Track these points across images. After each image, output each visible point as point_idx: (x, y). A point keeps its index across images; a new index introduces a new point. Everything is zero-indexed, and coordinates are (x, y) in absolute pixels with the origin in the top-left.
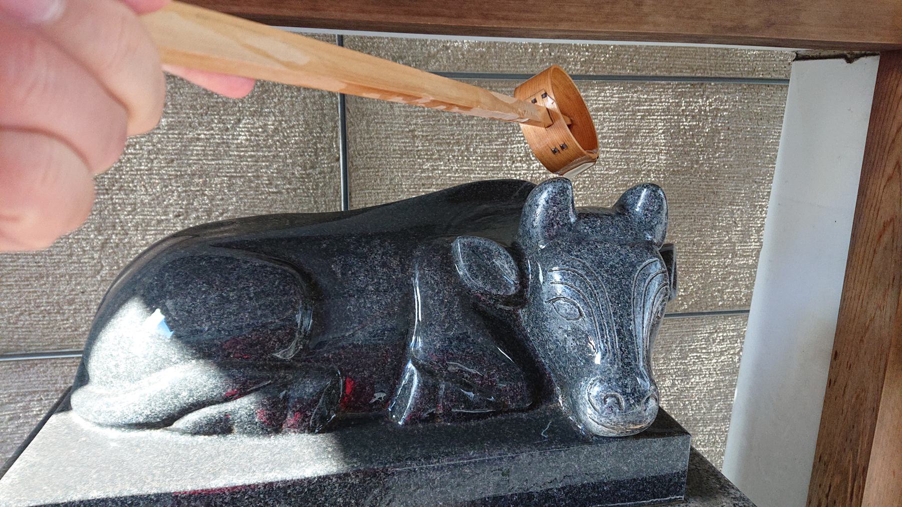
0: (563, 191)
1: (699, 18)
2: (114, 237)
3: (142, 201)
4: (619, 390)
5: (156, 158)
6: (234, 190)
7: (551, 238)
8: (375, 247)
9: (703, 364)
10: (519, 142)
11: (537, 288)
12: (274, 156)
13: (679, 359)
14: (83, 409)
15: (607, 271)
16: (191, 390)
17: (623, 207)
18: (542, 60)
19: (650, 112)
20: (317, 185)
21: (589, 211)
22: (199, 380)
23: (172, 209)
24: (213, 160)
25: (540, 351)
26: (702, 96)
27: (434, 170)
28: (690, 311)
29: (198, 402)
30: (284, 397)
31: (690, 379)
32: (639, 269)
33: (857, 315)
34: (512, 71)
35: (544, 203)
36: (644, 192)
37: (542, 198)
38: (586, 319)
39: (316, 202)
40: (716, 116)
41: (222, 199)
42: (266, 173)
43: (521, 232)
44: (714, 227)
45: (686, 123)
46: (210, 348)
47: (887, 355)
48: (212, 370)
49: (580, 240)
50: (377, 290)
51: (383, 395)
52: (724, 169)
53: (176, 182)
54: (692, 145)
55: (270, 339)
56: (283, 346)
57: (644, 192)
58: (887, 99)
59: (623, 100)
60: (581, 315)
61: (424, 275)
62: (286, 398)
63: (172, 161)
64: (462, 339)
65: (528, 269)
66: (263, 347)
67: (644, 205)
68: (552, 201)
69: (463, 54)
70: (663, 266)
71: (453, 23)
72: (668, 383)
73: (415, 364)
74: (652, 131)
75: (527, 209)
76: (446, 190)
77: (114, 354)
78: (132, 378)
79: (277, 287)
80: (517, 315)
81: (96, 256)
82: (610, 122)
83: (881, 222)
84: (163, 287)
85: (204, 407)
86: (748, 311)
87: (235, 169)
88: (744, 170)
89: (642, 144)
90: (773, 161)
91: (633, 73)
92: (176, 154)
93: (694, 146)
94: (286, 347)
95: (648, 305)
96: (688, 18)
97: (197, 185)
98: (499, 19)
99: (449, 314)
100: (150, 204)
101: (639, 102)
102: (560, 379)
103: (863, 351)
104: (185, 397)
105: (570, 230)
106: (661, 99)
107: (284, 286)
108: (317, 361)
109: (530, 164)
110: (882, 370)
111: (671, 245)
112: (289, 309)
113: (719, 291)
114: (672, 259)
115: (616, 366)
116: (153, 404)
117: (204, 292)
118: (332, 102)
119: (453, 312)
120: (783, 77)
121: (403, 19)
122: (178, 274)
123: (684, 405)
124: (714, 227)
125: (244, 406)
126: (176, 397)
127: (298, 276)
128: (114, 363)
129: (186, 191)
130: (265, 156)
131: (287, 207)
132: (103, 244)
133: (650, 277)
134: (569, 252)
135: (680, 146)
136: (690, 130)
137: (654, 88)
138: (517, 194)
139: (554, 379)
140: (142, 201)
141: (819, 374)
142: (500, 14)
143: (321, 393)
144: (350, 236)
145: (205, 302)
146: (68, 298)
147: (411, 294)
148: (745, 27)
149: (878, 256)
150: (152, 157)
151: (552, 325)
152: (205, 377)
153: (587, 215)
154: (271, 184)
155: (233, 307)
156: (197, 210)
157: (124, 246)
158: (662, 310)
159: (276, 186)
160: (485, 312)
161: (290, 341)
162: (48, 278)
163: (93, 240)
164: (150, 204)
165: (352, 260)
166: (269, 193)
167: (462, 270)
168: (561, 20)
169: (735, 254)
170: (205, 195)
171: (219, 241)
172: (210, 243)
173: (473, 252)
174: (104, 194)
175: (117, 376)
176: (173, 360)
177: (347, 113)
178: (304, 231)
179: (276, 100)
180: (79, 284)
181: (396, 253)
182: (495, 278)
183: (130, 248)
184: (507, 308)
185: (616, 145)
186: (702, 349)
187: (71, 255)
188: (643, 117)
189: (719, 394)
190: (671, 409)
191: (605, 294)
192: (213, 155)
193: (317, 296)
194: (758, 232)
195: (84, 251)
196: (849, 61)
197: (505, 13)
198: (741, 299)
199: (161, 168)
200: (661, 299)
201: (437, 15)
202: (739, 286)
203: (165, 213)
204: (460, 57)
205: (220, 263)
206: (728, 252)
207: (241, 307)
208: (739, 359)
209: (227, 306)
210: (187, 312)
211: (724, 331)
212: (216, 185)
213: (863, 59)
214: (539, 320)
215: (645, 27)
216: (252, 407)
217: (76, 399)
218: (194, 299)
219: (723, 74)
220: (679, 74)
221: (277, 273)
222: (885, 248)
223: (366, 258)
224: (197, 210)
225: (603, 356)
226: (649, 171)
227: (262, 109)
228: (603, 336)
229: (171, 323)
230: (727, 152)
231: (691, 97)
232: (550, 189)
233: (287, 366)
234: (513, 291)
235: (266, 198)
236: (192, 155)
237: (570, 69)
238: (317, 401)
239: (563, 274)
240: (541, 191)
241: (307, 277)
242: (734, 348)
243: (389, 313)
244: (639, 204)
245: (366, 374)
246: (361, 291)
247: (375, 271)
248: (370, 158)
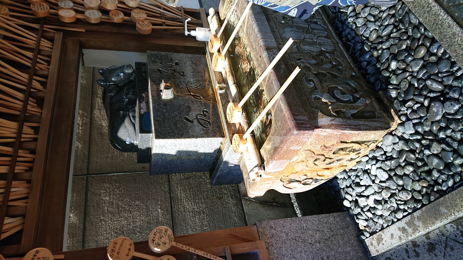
59: (98, 109)
101: (99, 105)
104: (130, 123)
125: (131, 114)
166: (124, 191)
199: (116, 218)
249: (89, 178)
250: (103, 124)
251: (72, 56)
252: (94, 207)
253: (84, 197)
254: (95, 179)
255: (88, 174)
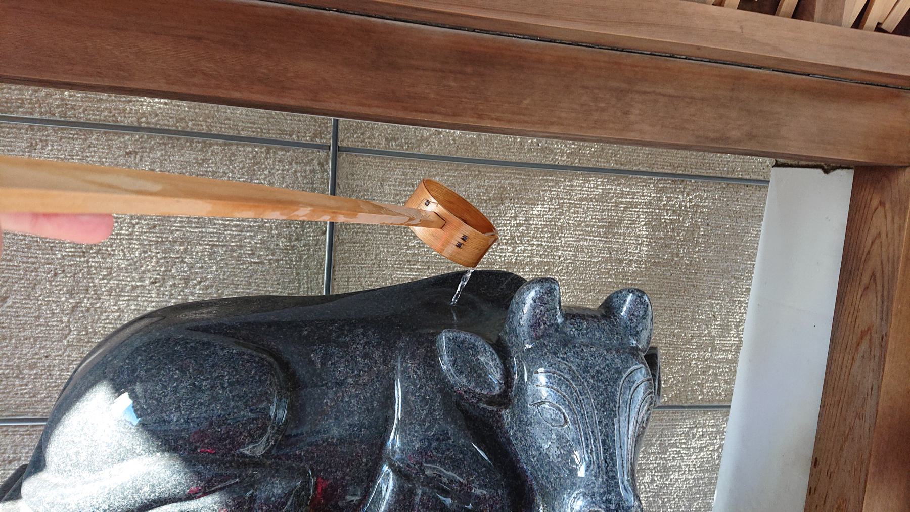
0: (550, 291)
1: (683, 129)
2: (86, 301)
3: (119, 265)
4: (602, 506)
5: (137, 224)
6: (215, 259)
7: (538, 338)
8: (358, 336)
9: (682, 460)
10: (505, 225)
11: (521, 390)
12: (259, 227)
13: (658, 453)
14: (34, 500)
15: (593, 377)
16: (153, 486)
17: (609, 309)
18: (530, 150)
19: (632, 205)
20: (301, 258)
21: (575, 311)
22: (162, 475)
23: (149, 275)
24: (196, 227)
25: (522, 456)
26: (682, 192)
27: (420, 247)
28: (670, 404)
29: (159, 499)
30: (249, 498)
31: (669, 475)
32: (625, 375)
33: (837, 422)
34: (501, 158)
35: (532, 302)
36: (630, 297)
37: (530, 296)
38: (571, 427)
39: (298, 274)
40: (696, 211)
41: (202, 268)
42: (250, 243)
43: (507, 328)
44: (694, 320)
45: (667, 217)
46: (176, 441)
47: (868, 466)
48: (177, 465)
49: (567, 342)
50: (356, 383)
51: (356, 499)
52: (705, 265)
53: (156, 248)
54: (673, 238)
55: (241, 433)
56: (254, 441)
57: (630, 297)
58: (862, 212)
59: (606, 192)
60: (566, 422)
61: (407, 368)
62: (252, 499)
63: (155, 227)
64: (442, 437)
65: (513, 368)
66: (232, 443)
67: (630, 310)
68: (539, 300)
69: (454, 140)
70: (648, 374)
71: (449, 121)
72: (647, 479)
73: (391, 466)
74: (634, 222)
75: (515, 306)
76: (433, 278)
77: (76, 440)
78: (93, 469)
79: (253, 377)
80: (501, 416)
81: (65, 319)
82: (593, 211)
83: (858, 331)
84: (134, 371)
85: (165, 504)
86: (729, 407)
87: (219, 237)
88: (724, 265)
89: (624, 234)
90: (752, 257)
91: (618, 167)
92: (159, 220)
93: (675, 239)
94: (256, 442)
95: (633, 414)
96: (673, 128)
97: (178, 252)
98: (492, 119)
99: (431, 412)
100: (126, 269)
101: (623, 194)
102: (542, 487)
103: (843, 460)
105: (556, 330)
106: (644, 192)
107: (260, 376)
108: (288, 458)
109: (514, 248)
110: (863, 480)
111: (655, 348)
112: (262, 402)
113: (698, 384)
114: (656, 364)
115: (600, 479)
116: (112, 498)
117: (176, 380)
118: (322, 178)
119: (434, 410)
120: (761, 178)
121: (401, 115)
122: (151, 358)
123: (663, 502)
124: (694, 320)
126: (137, 491)
127: (275, 365)
128: (75, 450)
129: (165, 258)
130: (250, 227)
131: (268, 278)
132: (73, 307)
133: (635, 385)
134: (555, 354)
135: (661, 238)
136: (671, 223)
137: (637, 183)
138: (504, 286)
139: (535, 487)
140: (119, 265)
141: (800, 481)
142: (493, 115)
143: (290, 494)
144: (333, 322)
145: (176, 391)
146: (29, 362)
147: (391, 388)
148: (728, 138)
149: (858, 363)
150: (134, 222)
151: (537, 430)
152: (169, 472)
153: (574, 316)
154: (253, 254)
155: (205, 397)
156: (174, 278)
157: (95, 310)
158: (647, 419)
159: (259, 257)
160: (466, 411)
161: (261, 436)
162: (11, 340)
163: (63, 303)
164: (126, 269)
165: (333, 349)
167: (445, 365)
168: (552, 124)
169: (714, 348)
170: (185, 262)
171: (195, 324)
172: (188, 325)
173: (458, 347)
174: (80, 257)
175: (77, 465)
176: (137, 451)
177: (337, 188)
178: (287, 315)
179: (266, 172)
180: (43, 348)
181: (379, 344)
182: (479, 376)
183: (101, 313)
184: (490, 408)
185: (599, 233)
186: (681, 444)
187: (38, 317)
188: (625, 209)
189: (698, 492)
190: (649, 506)
191: (590, 402)
192: (198, 223)
193: (293, 385)
194: (737, 327)
195: (53, 314)
196: (826, 172)
197: (498, 115)
198: (720, 394)
199: (142, 233)
200: (645, 408)
201: (433, 112)
202: (718, 380)
203: (141, 279)
204: (452, 142)
205: (196, 349)
206: (707, 345)
207: (213, 397)
208: (718, 456)
209: (198, 395)
210: (156, 400)
211: (704, 426)
212: (197, 252)
213: (838, 171)
214: (522, 423)
215: (632, 134)
216: (216, 508)
217: (28, 486)
218: (165, 387)
219: (703, 173)
220: (661, 171)
221: (255, 361)
222: (863, 357)
223: (348, 347)
224: (174, 278)
225: (588, 467)
226: (631, 261)
227: (251, 180)
228: (587, 446)
229: (138, 410)
230: (707, 247)
231: (671, 193)
232: (537, 289)
233: (255, 463)
234: (497, 391)
235: (247, 268)
236: (175, 222)
237: (557, 160)
238: (285, 504)
239: (549, 377)
240: (529, 289)
241: (285, 366)
242: (713, 444)
243: (368, 410)
244: (625, 309)
245: (339, 474)
246: (340, 384)
247: (356, 362)
248: (357, 233)
249: (322, 154)
250: (539, 208)
251: (801, 124)
252: (201, 165)
253: (243, 134)
254: (313, 171)
255: (337, 149)
